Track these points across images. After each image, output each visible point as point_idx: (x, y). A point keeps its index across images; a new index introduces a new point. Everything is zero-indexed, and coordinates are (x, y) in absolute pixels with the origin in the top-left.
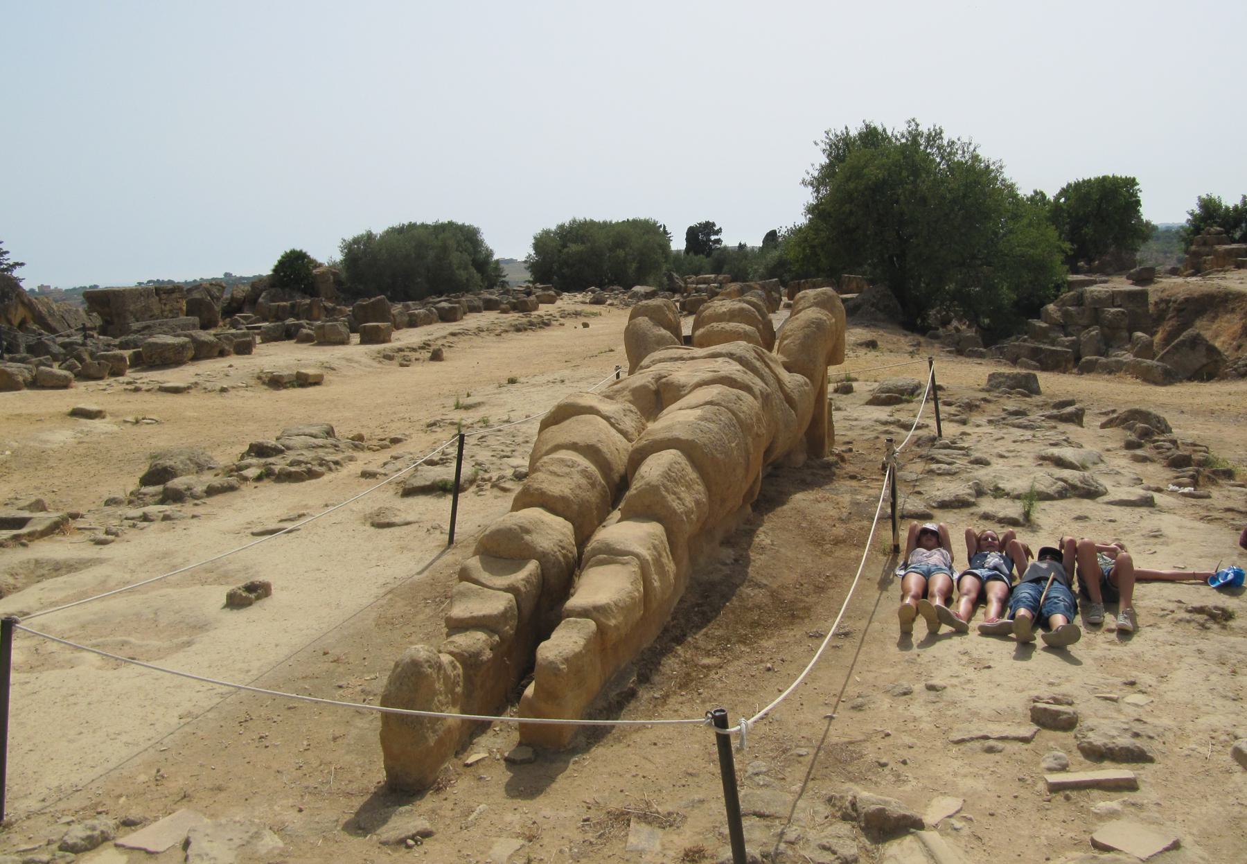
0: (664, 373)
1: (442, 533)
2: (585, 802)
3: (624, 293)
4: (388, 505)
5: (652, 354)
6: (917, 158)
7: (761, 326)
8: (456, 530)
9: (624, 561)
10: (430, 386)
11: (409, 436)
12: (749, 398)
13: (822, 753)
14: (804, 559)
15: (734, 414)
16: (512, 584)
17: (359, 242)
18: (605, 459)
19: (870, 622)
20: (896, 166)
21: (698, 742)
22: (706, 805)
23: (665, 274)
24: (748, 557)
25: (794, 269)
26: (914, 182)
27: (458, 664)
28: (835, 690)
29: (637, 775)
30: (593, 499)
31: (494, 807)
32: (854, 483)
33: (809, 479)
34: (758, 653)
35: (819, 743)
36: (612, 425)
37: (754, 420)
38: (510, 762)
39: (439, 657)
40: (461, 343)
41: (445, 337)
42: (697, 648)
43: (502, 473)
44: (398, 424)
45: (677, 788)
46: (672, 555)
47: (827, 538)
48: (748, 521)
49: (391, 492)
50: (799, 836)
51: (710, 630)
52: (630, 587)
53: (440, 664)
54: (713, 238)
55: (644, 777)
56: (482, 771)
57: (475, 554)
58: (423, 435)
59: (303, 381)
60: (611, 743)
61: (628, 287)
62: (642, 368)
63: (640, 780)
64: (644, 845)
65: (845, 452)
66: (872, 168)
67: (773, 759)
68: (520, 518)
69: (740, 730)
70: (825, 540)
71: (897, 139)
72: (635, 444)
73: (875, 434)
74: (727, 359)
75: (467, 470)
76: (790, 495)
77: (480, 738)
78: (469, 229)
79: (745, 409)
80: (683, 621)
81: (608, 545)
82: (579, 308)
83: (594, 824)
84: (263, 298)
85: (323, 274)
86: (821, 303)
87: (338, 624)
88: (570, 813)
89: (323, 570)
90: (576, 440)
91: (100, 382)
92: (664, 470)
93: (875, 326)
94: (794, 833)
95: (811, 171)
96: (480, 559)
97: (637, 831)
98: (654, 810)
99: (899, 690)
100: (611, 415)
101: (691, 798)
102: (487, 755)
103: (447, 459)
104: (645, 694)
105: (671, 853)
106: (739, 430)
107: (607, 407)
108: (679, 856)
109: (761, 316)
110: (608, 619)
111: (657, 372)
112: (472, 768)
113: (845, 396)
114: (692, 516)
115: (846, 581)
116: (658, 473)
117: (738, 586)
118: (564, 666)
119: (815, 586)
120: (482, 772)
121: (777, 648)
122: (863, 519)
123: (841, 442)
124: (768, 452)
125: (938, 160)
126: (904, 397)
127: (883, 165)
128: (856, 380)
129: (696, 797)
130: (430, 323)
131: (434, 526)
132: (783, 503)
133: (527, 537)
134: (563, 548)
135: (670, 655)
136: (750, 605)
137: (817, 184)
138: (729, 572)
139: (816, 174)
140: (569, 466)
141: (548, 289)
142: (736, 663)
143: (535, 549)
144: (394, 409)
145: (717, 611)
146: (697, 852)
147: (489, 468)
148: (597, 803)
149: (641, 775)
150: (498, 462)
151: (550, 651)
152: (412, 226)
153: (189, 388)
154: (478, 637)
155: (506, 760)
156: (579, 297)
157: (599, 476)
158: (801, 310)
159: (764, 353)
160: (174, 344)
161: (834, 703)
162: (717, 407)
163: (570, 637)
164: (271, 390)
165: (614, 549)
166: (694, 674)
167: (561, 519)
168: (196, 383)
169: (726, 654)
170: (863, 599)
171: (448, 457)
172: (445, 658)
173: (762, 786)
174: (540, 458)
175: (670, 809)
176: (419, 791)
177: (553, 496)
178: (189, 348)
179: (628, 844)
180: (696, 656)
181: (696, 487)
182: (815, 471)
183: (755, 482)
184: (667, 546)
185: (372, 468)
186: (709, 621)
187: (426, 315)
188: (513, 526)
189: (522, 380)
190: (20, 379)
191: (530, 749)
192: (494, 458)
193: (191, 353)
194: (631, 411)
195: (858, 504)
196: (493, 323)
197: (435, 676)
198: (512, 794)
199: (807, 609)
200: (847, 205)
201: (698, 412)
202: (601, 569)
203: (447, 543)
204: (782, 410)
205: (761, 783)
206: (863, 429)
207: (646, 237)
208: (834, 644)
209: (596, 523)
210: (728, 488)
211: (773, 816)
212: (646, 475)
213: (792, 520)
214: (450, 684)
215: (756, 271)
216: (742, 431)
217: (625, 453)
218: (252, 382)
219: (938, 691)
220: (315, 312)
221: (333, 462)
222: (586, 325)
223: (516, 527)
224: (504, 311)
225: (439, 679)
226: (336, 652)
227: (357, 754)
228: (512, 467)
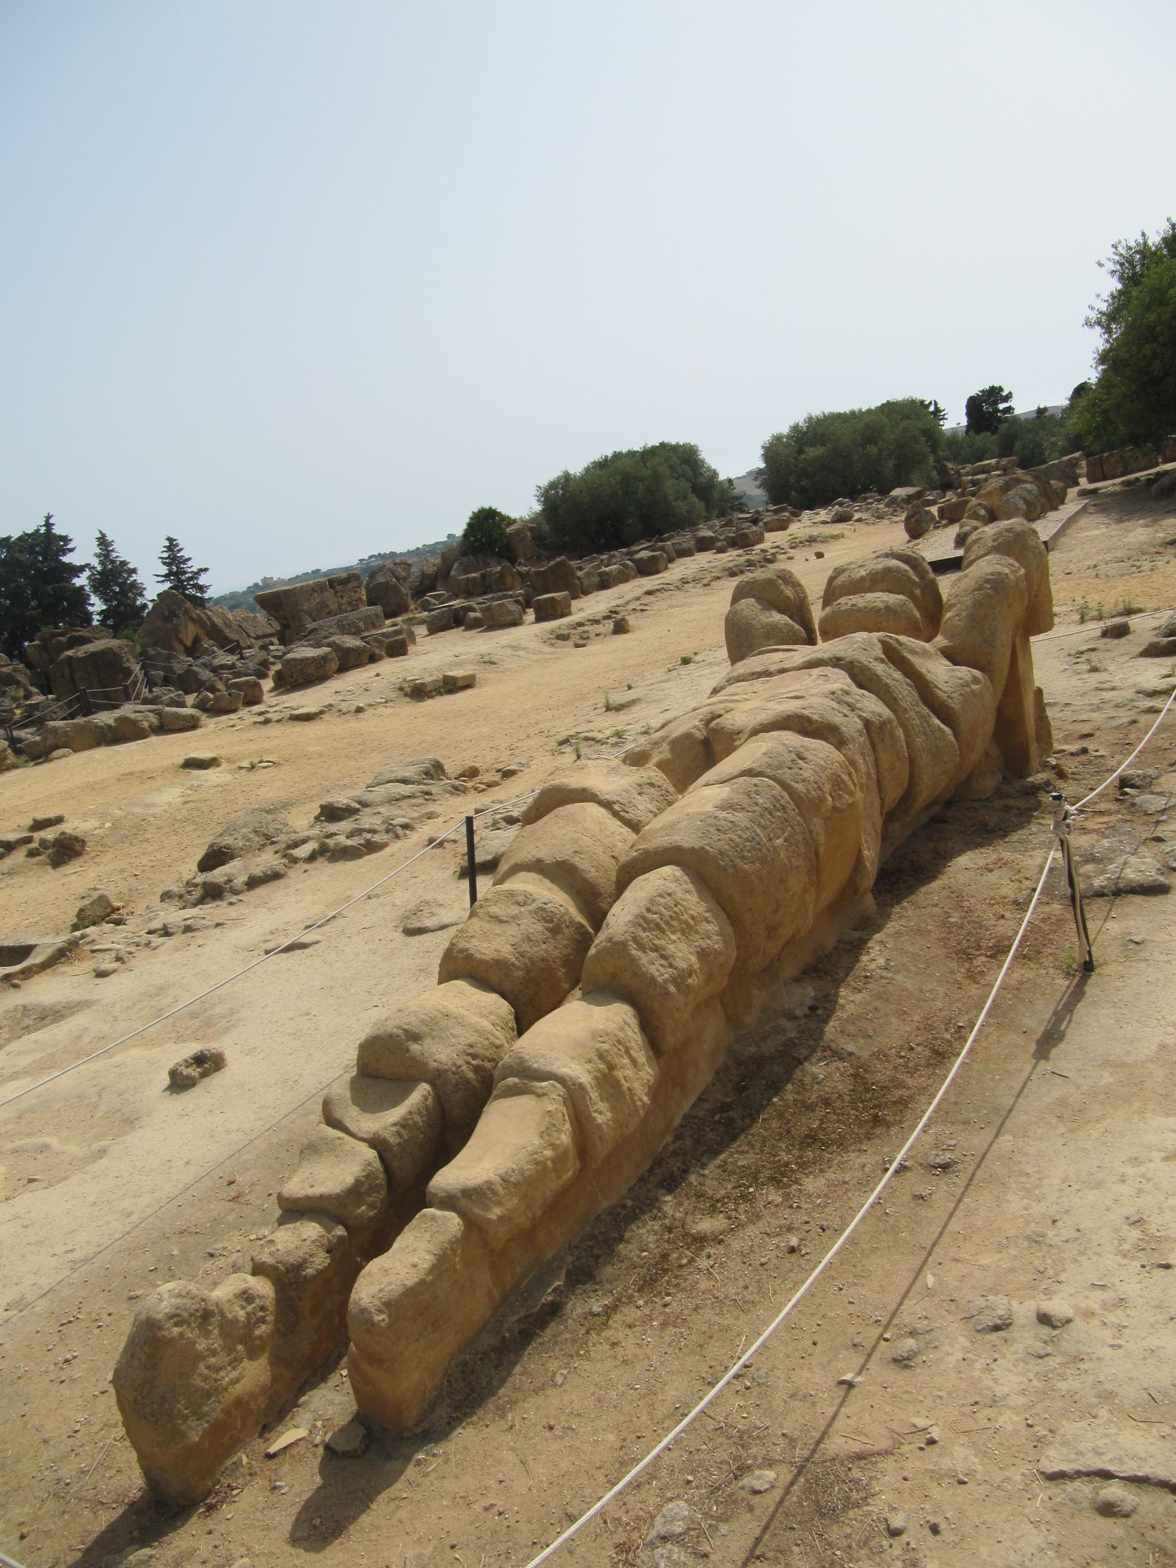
3: (879, 501)
7: (918, 592)
9: (540, 1091)
14: (931, 991)
15: (784, 786)
17: (557, 487)
18: (585, 880)
19: (996, 1136)
33: (993, 820)
36: (616, 814)
40: (658, 604)
41: (638, 599)
47: (983, 944)
51: (731, 1155)
54: (1001, 406)
59: (451, 686)
61: (884, 491)
76: (950, 859)
82: (815, 532)
84: (456, 570)
85: (518, 531)
91: (232, 716)
92: (636, 911)
99: (988, 1320)
100: (614, 798)
104: (578, 1307)
110: (487, 1208)
113: (1116, 641)
130: (627, 580)
132: (933, 877)
133: (415, 1048)
135: (646, 1217)
137: (1107, 321)
139: (1104, 307)
140: (518, 904)
141: (784, 510)
143: (426, 1064)
152: (617, 456)
153: (322, 712)
158: (973, 561)
160: (313, 657)
161: (869, 1344)
164: (414, 702)
168: (331, 705)
177: (483, 962)
178: (332, 660)
187: (620, 572)
188: (395, 1031)
190: (146, 725)
193: (335, 665)
204: (925, 733)
209: (566, 986)
215: (1054, 444)
218: (393, 695)
219: (1054, 1327)
220: (509, 580)
221: (401, 826)
222: (820, 555)
223: (400, 1031)
224: (721, 550)
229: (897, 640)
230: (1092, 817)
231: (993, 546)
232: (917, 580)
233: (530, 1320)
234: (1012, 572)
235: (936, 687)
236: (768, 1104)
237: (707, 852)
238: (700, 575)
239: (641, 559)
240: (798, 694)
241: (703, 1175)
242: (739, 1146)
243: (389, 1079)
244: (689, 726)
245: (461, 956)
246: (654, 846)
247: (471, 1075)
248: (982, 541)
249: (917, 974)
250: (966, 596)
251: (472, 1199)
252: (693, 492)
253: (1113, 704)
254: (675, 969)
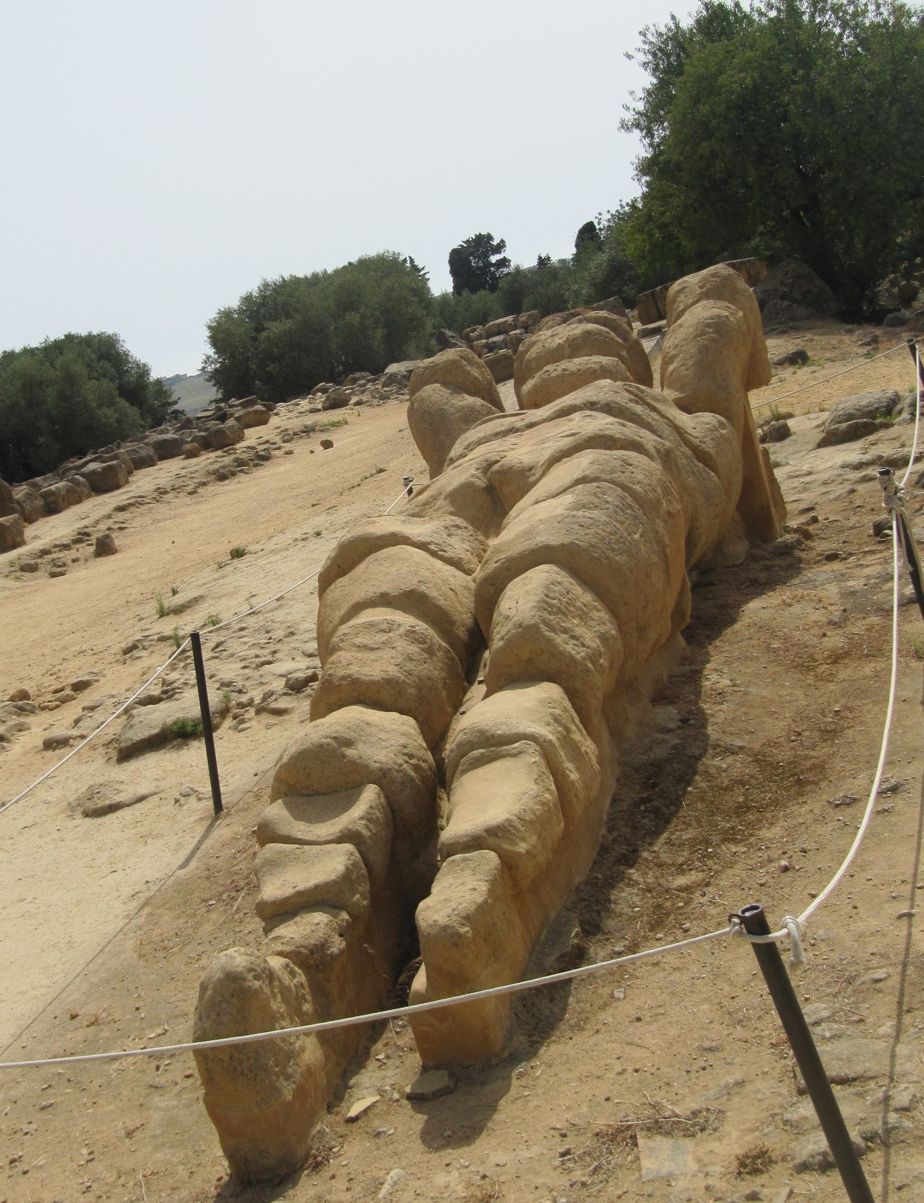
0: (493, 457)
1: (199, 799)
2: (554, 1129)
4: (101, 780)
5: (463, 436)
6: (803, 36)
7: (624, 353)
8: (222, 789)
9: (515, 751)
10: (108, 594)
11: (100, 673)
12: (643, 459)
13: (910, 970)
14: (790, 695)
16: (347, 829)
18: (438, 608)
20: (770, 59)
21: (706, 1000)
22: (748, 1088)
23: (432, 335)
24: (702, 712)
25: (129, 1077)
26: (806, 78)
27: (296, 969)
28: (903, 873)
29: (624, 1070)
30: (436, 673)
31: (414, 1169)
32: (836, 566)
33: (762, 576)
34: (760, 849)
35: (901, 958)
36: (434, 554)
37: (659, 490)
38: (417, 1099)
39: (266, 961)
40: (137, 520)
41: (109, 516)
42: (661, 866)
43: (267, 688)
44: (77, 662)
45: (693, 1075)
46: (586, 729)
48: (685, 660)
49: (100, 761)
50: (914, 1096)
51: (672, 833)
52: (535, 787)
53: (269, 970)
54: (494, 259)
55: (637, 1071)
56: (376, 1123)
57: (273, 800)
58: (121, 667)
60: (568, 1034)
61: (377, 370)
62: (452, 461)
63: (630, 1077)
64: (667, 1167)
65: (808, 524)
66: (732, 73)
67: (835, 996)
68: (331, 725)
69: (788, 935)
70: (816, 661)
71: (761, 14)
72: (479, 573)
73: (847, 487)
74: (588, 412)
75: (214, 697)
77: (358, 1076)
78: (100, 341)
79: (640, 477)
80: (626, 830)
81: (482, 732)
82: (310, 420)
83: (579, 1157)
86: (712, 292)
87: (78, 971)
88: (535, 1150)
89: (30, 899)
90: (384, 588)
92: (538, 598)
93: (796, 329)
94: (905, 1093)
95: (632, 105)
96: (285, 803)
97: (651, 1150)
98: (667, 1114)
100: (428, 539)
101: (722, 1083)
102: (378, 1097)
103: (173, 689)
105: (717, 1169)
106: (640, 512)
107: (418, 530)
108: (730, 1170)
109: (619, 335)
110: (515, 844)
111: (482, 458)
112: (360, 1122)
113: (779, 444)
114: (602, 661)
115: (869, 712)
116: (530, 605)
117: (698, 759)
118: (466, 929)
119: (821, 730)
120: (377, 1124)
121: (789, 835)
122: (867, 614)
123: (796, 512)
124: (690, 541)
125: (837, 31)
126: (878, 421)
127: (748, 62)
128: (790, 416)
129: (730, 1080)
130: (79, 501)
131: (184, 792)
132: (732, 621)
134: (411, 756)
135: (621, 885)
136: (726, 782)
138: (677, 741)
139: (641, 106)
141: (252, 403)
142: (730, 872)
143: (367, 766)
144: (62, 643)
145: (676, 803)
146: (757, 1157)
147: (244, 686)
148: (574, 1125)
149: (630, 1069)
150: (256, 674)
151: (437, 911)
154: (316, 921)
155: (410, 1097)
156: (304, 404)
157: (435, 635)
158: (683, 312)
159: (642, 391)
162: (596, 484)
163: (463, 884)
165: (493, 736)
166: (668, 904)
167: (394, 715)
169: (710, 862)
170: (904, 732)
171: (175, 685)
172: (276, 963)
173: (831, 1038)
174: (335, 629)
175: (695, 1106)
176: (287, 1175)
177: (373, 682)
179: (644, 1172)
180: (663, 877)
181: (595, 615)
182: (767, 562)
183: (681, 593)
184: (575, 715)
185: (59, 732)
186: (668, 821)
188: (324, 740)
189: (252, 548)
191: (444, 1073)
192: (247, 671)
194: (458, 527)
195: (853, 593)
196: (178, 476)
197: (267, 990)
198: (436, 1145)
199: (820, 768)
200: (705, 144)
201: (568, 498)
202: (480, 772)
203: (213, 811)
204: (693, 473)
205: (828, 1034)
206: (825, 483)
207: (387, 282)
208: (880, 809)
210: (645, 607)
211: (862, 1077)
212: (512, 613)
213: (754, 642)
214: (292, 1000)
215: (577, 293)
216: (645, 514)
217: (465, 592)
223: (328, 740)
224: (191, 455)
225: (275, 997)
226: (90, 1009)
227: (171, 1147)
228: (281, 676)
229: (638, 388)
230: (864, 557)
231: (702, 293)
232: (621, 341)
233: (566, 959)
234: (732, 314)
235: (686, 432)
236: (685, 794)
237: (578, 546)
238: (178, 483)
239: (93, 472)
240: (573, 431)
241: (654, 852)
242: (676, 826)
243: (324, 794)
244: (468, 474)
245: (344, 683)
246: (517, 552)
247: (412, 773)
248: (688, 290)
249: (767, 686)
250: (688, 344)
251: (498, 836)
252: (120, 395)
253: (820, 482)
254: (588, 647)
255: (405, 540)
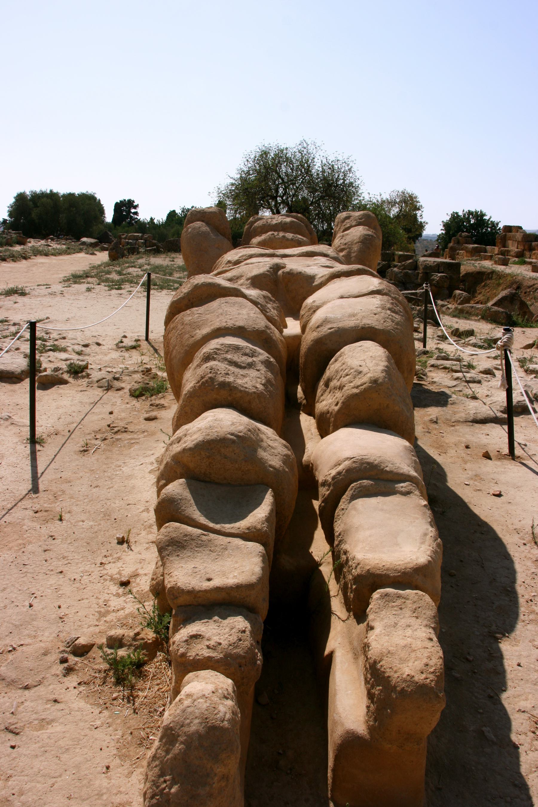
54: (133, 210)
255: (244, 296)
